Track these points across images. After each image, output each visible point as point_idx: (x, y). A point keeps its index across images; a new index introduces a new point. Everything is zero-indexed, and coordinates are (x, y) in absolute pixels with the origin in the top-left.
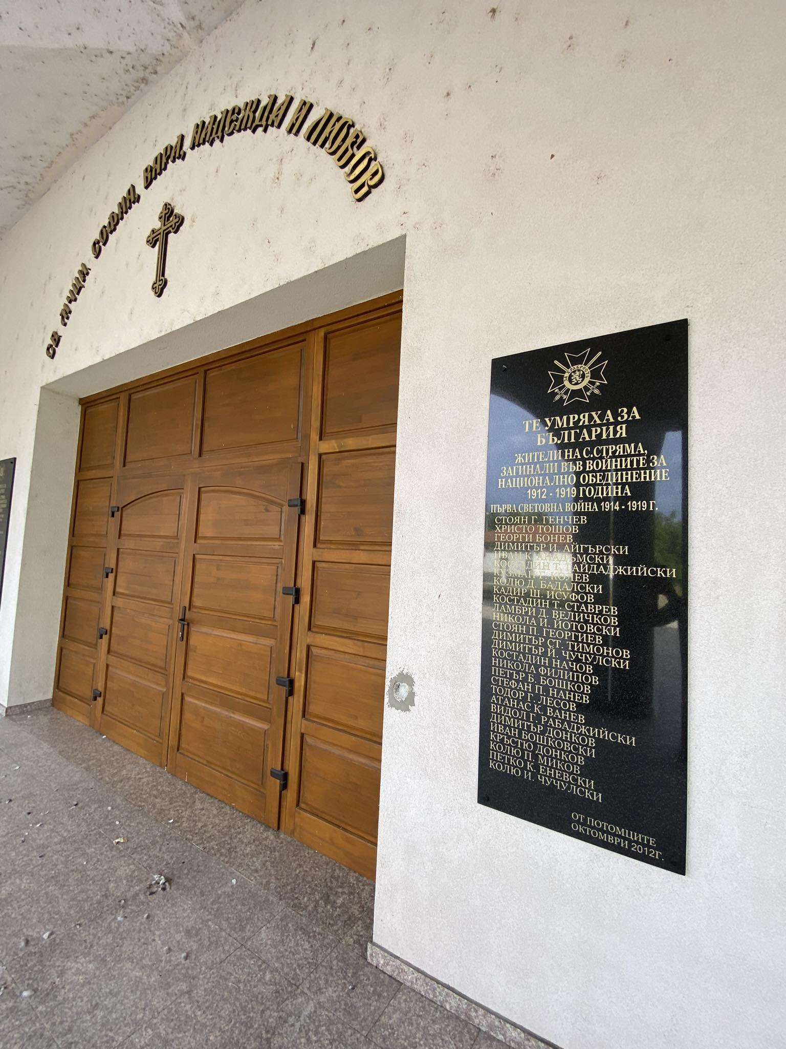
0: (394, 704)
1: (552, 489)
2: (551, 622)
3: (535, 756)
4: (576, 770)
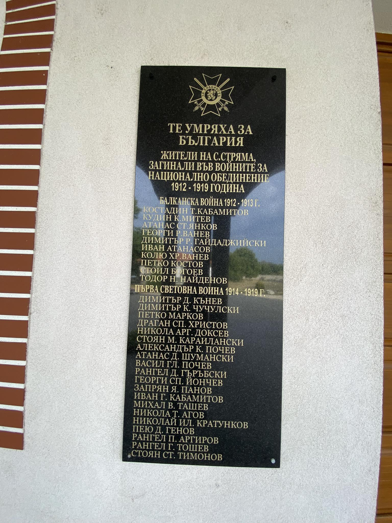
1: (190, 184)
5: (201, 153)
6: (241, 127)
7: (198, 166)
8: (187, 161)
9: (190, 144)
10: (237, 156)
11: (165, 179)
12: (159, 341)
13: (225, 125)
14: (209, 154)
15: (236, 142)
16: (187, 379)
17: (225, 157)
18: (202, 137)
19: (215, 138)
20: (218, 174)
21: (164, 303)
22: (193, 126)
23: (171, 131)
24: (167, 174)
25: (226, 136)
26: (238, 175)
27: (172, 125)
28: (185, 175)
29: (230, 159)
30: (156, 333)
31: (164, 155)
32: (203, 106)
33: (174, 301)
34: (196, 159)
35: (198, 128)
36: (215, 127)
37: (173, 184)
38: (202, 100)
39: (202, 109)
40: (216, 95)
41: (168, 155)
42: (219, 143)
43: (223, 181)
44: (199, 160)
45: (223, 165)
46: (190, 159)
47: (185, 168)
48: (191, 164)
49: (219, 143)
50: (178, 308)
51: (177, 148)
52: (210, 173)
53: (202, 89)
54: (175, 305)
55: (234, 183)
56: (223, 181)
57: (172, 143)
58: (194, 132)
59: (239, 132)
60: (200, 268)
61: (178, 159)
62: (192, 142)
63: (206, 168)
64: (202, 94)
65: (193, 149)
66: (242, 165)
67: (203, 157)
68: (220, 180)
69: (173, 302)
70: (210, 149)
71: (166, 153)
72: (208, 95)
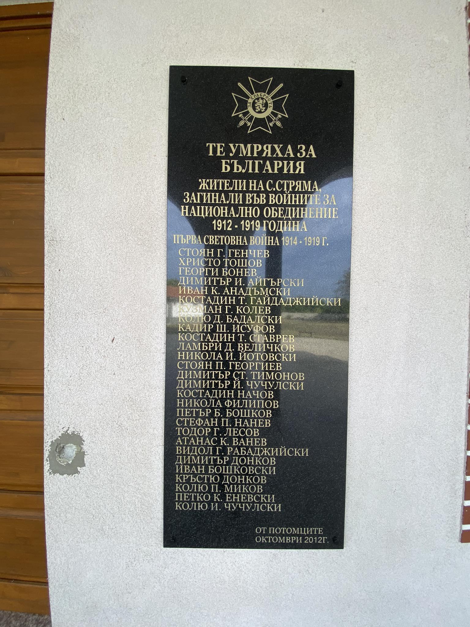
0: (57, 469)
1: (237, 221)
2: (236, 354)
3: (221, 487)
4: (260, 489)
5: (251, 181)
6: (301, 148)
7: (247, 198)
8: (233, 191)
9: (235, 171)
10: (297, 184)
11: (203, 215)
12: (204, 367)
13: (281, 145)
14: (261, 182)
15: (295, 168)
16: (235, 382)
17: (281, 186)
18: (251, 162)
19: (268, 163)
20: (273, 208)
21: (208, 379)
22: (239, 146)
23: (211, 154)
24: (205, 208)
25: (282, 159)
26: (298, 209)
27: (211, 145)
28: (229, 210)
29: (288, 188)
30: (201, 358)
31: (203, 185)
32: (250, 120)
33: (221, 376)
34: (245, 189)
35: (245, 150)
36: (267, 148)
37: (214, 222)
38: (248, 112)
39: (249, 124)
40: (266, 105)
41: (208, 184)
42: (273, 169)
43: (280, 216)
44: (248, 191)
45: (279, 196)
46: (236, 189)
47: (231, 201)
48: (239, 195)
49: (273, 169)
50: (226, 375)
51: (217, 174)
52: (262, 207)
53: (248, 98)
54: (223, 381)
55: (293, 219)
56: (280, 216)
57: (212, 169)
58: (241, 155)
59: (298, 154)
60: (268, 418)
61: (221, 189)
62: (238, 168)
63: (257, 200)
64: (248, 104)
65: (240, 176)
66: (304, 196)
67: (253, 187)
68: (275, 215)
69: (220, 378)
70: (262, 176)
71: (205, 181)
72: (256, 105)
